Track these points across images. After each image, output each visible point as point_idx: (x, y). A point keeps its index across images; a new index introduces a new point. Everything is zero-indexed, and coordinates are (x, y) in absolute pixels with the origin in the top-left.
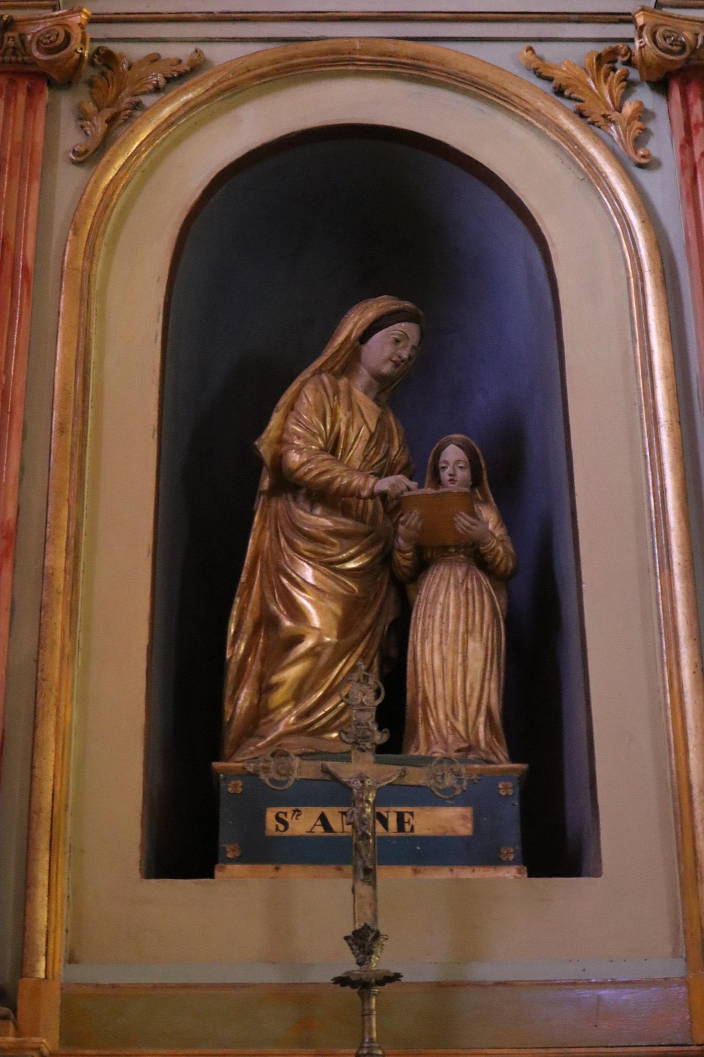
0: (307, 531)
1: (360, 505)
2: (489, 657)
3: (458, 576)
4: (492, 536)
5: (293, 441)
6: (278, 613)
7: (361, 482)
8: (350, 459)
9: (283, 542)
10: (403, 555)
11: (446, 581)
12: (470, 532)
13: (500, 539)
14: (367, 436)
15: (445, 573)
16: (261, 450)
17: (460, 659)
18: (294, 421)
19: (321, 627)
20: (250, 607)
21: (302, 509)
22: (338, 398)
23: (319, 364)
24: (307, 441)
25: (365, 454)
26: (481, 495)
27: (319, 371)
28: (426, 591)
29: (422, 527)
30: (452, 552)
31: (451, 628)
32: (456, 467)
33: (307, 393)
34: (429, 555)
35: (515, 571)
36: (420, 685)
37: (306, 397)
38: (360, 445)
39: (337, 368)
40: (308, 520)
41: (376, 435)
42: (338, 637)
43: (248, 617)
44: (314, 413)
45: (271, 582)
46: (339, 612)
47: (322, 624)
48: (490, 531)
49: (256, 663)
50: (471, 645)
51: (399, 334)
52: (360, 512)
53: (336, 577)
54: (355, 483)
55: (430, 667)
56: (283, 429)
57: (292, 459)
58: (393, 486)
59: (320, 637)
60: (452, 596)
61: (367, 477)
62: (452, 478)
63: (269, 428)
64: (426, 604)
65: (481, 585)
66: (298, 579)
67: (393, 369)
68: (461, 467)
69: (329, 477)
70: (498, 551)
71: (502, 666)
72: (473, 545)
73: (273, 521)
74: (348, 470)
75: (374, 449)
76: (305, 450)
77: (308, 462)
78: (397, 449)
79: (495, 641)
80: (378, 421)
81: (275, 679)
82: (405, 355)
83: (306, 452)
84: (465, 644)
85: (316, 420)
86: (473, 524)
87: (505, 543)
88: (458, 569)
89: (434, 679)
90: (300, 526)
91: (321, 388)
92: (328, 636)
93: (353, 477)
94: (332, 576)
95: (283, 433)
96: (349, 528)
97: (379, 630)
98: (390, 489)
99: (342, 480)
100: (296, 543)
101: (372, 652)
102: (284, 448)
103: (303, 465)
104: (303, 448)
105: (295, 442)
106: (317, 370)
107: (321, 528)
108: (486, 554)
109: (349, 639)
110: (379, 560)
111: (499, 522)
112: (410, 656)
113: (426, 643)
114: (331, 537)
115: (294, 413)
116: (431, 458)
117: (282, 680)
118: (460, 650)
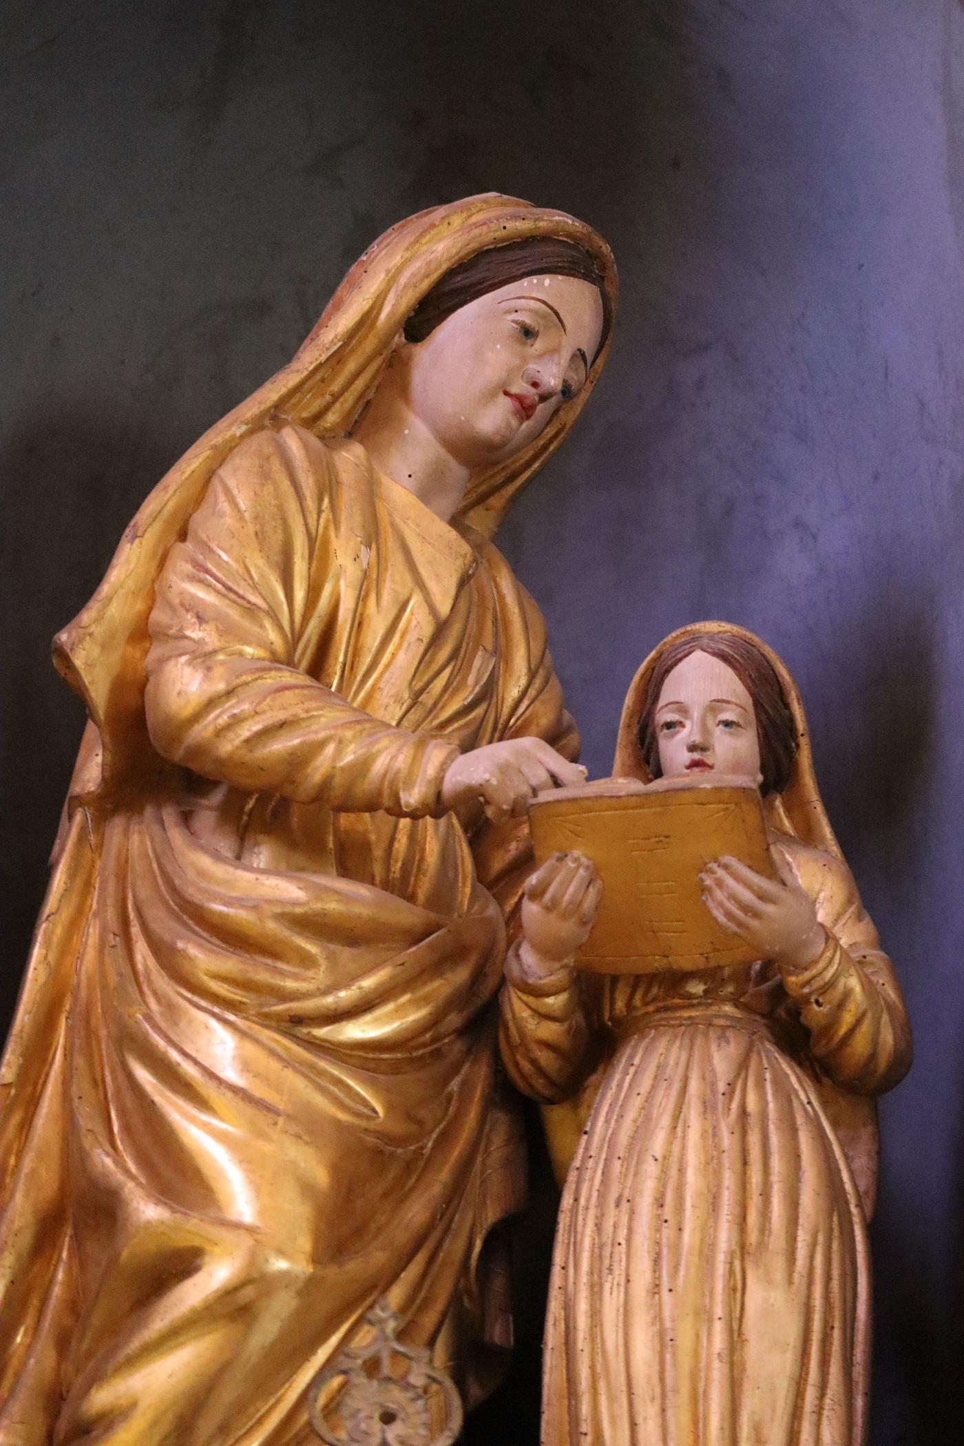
0: (221, 915)
1: (396, 845)
2: (816, 1337)
3: (713, 1071)
4: (827, 939)
5: (181, 629)
6: (120, 1177)
7: (402, 761)
8: (370, 696)
9: (141, 950)
10: (530, 1000)
11: (676, 1086)
12: (754, 923)
13: (855, 955)
14: (427, 629)
15: (671, 1062)
16: (78, 661)
17: (719, 1341)
18: (188, 568)
19: (258, 1223)
20: (28, 1163)
21: (205, 850)
22: (333, 507)
23: (274, 397)
24: (227, 630)
25: (418, 685)
26: (790, 818)
27: (274, 417)
28: (607, 1121)
29: (598, 907)
30: (690, 996)
31: (689, 1237)
32: (710, 723)
33: (232, 483)
34: (620, 1004)
35: (902, 1062)
36: (585, 1427)
37: (228, 492)
38: (401, 656)
39: (332, 418)
40: (227, 883)
41: (456, 629)
42: (315, 1259)
43: (19, 1198)
44: (255, 544)
45: (98, 1083)
46: (321, 1176)
47: (262, 1213)
48: (821, 925)
49: (39, 1347)
50: (755, 1296)
51: (531, 310)
52: (397, 867)
53: (312, 1067)
54: (379, 766)
55: (617, 1365)
56: (153, 592)
57: (178, 687)
58: (504, 769)
59: (254, 1257)
60: (694, 1136)
61: (421, 745)
62: (697, 756)
63: (105, 589)
64: (608, 1161)
65: (790, 1101)
66: (188, 1068)
67: (514, 422)
68: (727, 724)
69: (296, 741)
70: (848, 993)
71: (859, 1371)
72: (763, 976)
73: (111, 888)
74: (358, 722)
75: (446, 674)
76: (221, 657)
77: (229, 693)
78: (523, 681)
79: (835, 1284)
80: (463, 582)
81: (101, 1398)
82: (552, 376)
83: (222, 663)
84: (737, 1290)
85: (262, 568)
86: (763, 897)
87: (869, 970)
88: (714, 1047)
89: (631, 1404)
90: (197, 898)
91: (276, 466)
92: (281, 1253)
93: (372, 744)
94: (303, 1063)
95: (151, 609)
96: (357, 909)
97: (454, 1248)
98: (494, 782)
99: (339, 753)
100: (183, 954)
101: (429, 1320)
102: (155, 652)
103: (211, 703)
104: (214, 652)
105: (188, 633)
106: (262, 415)
107: (266, 907)
108: (806, 1000)
109: (356, 1267)
110: (454, 1020)
111: (849, 902)
112: (553, 1336)
113: (607, 1287)
114: (301, 934)
115: (189, 546)
116: (629, 700)
117: (123, 1402)
118: (719, 1311)
